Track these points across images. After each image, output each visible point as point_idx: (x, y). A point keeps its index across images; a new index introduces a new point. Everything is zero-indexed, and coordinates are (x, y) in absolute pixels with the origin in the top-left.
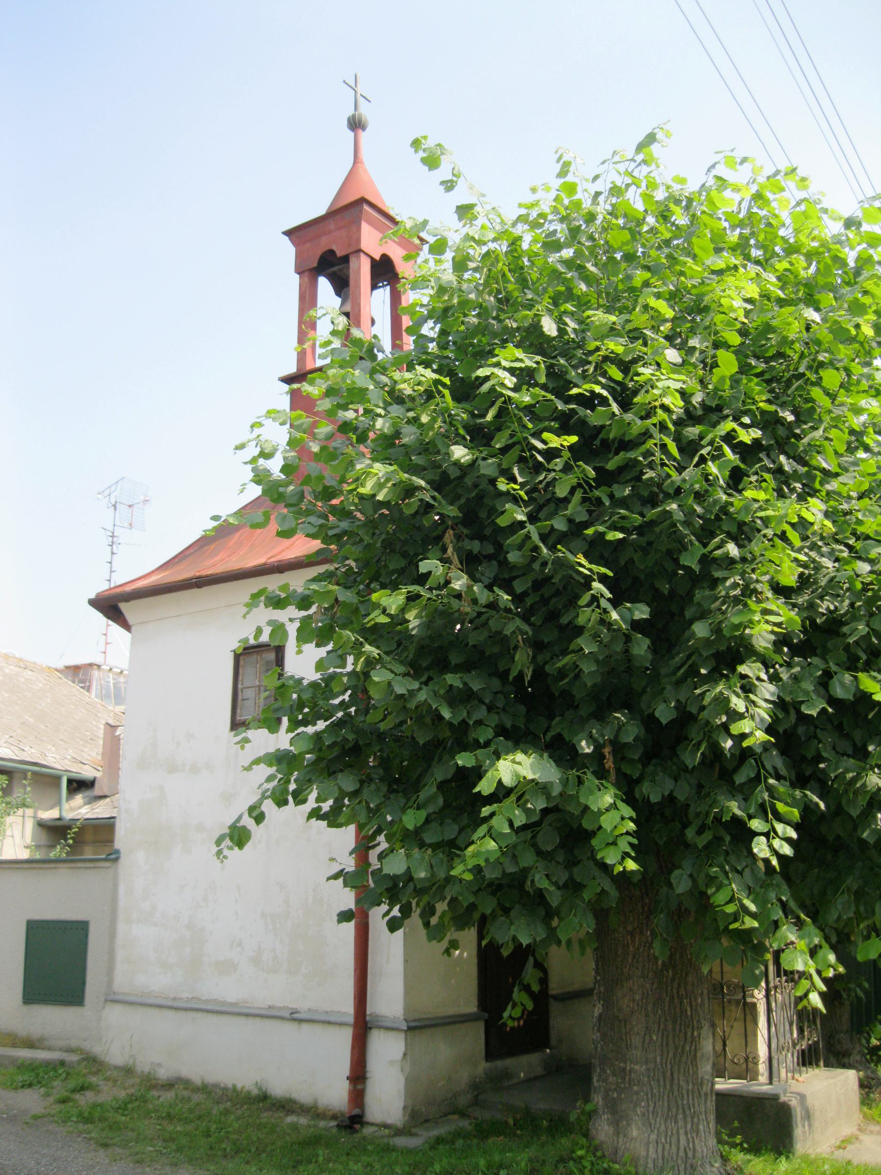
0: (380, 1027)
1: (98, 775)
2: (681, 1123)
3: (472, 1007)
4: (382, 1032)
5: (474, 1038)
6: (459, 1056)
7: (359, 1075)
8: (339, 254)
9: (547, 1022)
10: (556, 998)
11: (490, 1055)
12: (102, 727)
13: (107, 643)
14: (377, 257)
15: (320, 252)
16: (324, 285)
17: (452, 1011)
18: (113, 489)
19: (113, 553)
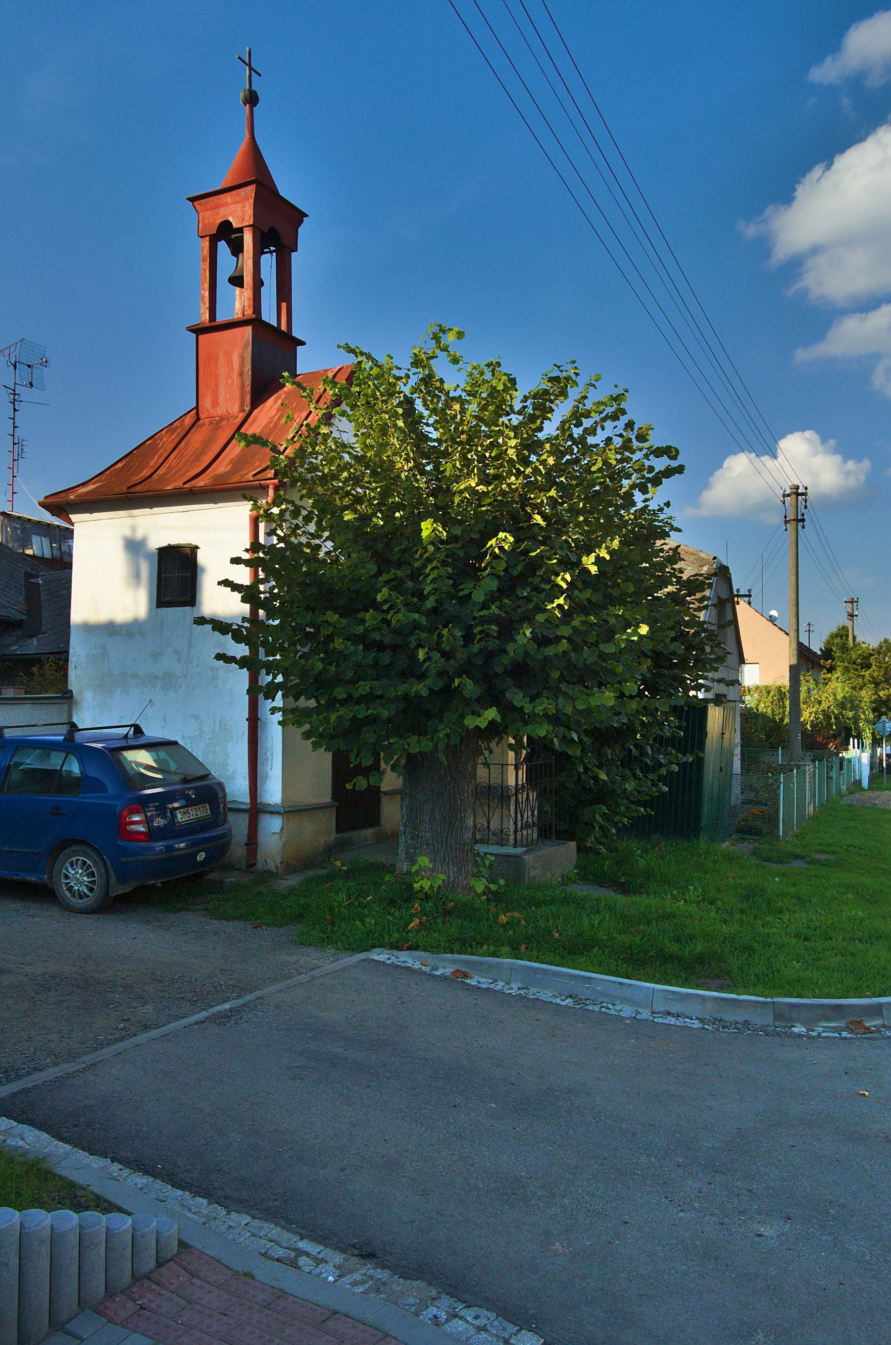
0: (266, 812)
1: (24, 618)
2: (451, 867)
3: (327, 798)
4: (268, 815)
5: (329, 820)
6: (319, 831)
7: (867, 304)
8: (235, 225)
9: (379, 811)
10: (385, 793)
11: (338, 831)
12: (22, 575)
13: (13, 493)
14: (266, 231)
15: (218, 221)
16: (222, 246)
17: (272, 816)
18: (12, 349)
19: (15, 410)
